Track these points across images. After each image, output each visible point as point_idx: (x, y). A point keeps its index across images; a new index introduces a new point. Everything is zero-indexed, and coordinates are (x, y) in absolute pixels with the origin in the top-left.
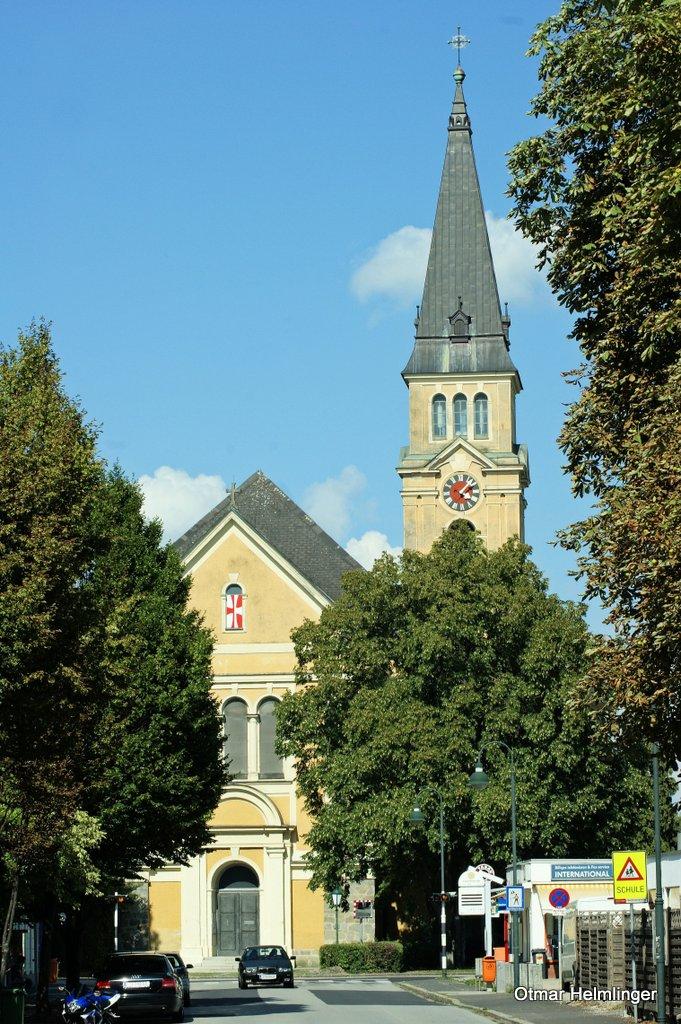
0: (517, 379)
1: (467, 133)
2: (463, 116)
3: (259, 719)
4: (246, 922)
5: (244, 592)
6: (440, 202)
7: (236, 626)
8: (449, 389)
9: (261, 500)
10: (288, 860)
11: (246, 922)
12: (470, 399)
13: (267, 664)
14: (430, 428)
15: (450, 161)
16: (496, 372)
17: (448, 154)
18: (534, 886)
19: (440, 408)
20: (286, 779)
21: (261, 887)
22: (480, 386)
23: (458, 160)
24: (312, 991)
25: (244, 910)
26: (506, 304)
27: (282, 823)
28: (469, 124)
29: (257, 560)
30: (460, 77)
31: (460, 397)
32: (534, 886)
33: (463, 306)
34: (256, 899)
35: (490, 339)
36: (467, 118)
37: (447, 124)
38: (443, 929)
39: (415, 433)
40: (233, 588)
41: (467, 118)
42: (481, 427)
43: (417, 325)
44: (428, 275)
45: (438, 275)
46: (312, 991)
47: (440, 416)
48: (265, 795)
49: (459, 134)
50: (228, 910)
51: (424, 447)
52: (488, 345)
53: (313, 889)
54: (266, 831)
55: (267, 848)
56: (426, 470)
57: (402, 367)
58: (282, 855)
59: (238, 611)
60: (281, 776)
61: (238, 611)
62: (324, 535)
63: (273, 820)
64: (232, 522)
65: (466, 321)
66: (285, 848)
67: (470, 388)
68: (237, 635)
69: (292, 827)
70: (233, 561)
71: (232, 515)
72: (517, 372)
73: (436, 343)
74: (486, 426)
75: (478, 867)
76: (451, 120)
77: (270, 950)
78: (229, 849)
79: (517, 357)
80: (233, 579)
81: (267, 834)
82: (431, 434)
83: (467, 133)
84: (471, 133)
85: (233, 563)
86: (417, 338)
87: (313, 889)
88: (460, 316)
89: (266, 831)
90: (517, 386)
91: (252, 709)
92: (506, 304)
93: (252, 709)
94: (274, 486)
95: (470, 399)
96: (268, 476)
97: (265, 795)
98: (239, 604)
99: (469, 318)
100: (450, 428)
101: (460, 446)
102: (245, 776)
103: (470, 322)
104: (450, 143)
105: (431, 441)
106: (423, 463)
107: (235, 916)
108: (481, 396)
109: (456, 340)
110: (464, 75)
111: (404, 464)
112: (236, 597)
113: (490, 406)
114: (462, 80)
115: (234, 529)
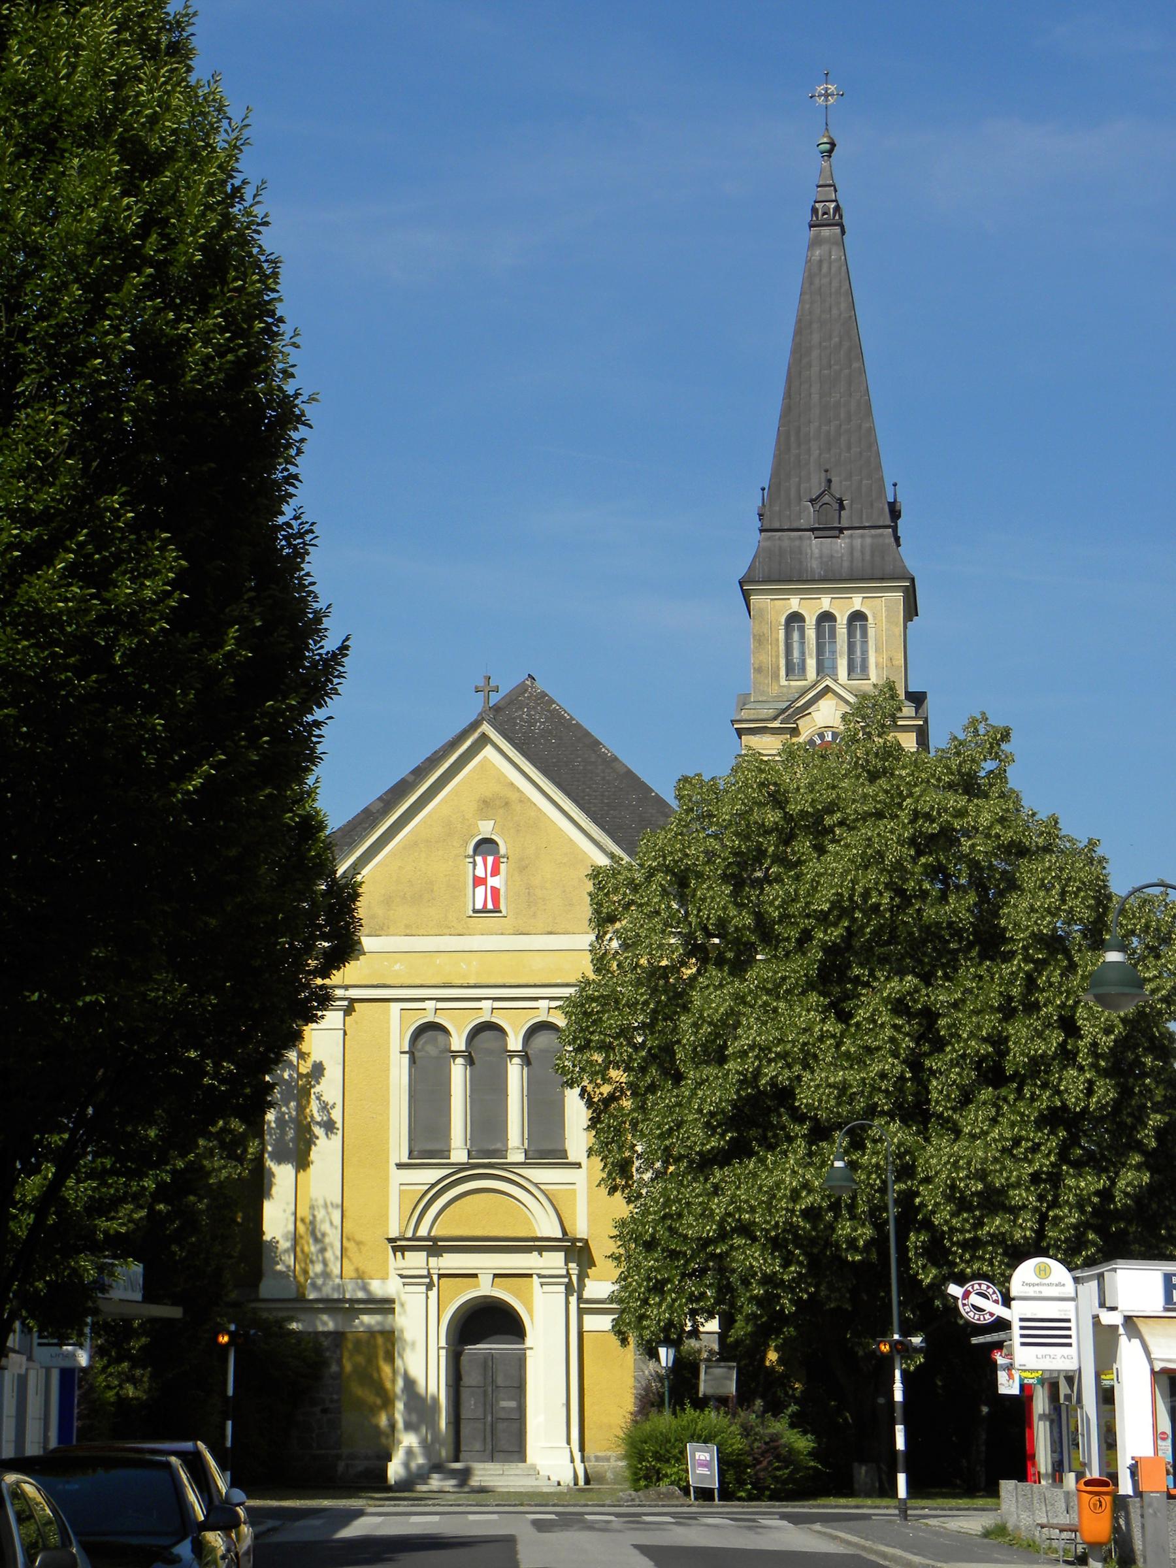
0: (911, 589)
1: (837, 230)
2: (833, 205)
3: (527, 1060)
4: (504, 1404)
5: (502, 851)
6: (798, 332)
7: (490, 906)
8: (811, 607)
9: (531, 723)
10: (573, 1299)
11: (504, 1404)
12: (842, 620)
13: (538, 969)
14: (782, 662)
15: (812, 273)
16: (882, 579)
17: (808, 261)
18: (1128, 1319)
19: (796, 636)
20: (571, 1159)
21: (529, 1341)
22: (857, 602)
23: (825, 269)
24: (636, 1546)
25: (500, 1381)
26: (895, 485)
27: (565, 1232)
28: (841, 217)
29: (524, 800)
30: (828, 147)
31: (826, 618)
32: (1128, 1319)
33: (833, 485)
34: (520, 1362)
35: (873, 532)
36: (837, 209)
37: (807, 216)
38: (898, 1414)
39: (759, 670)
40: (486, 845)
41: (837, 209)
42: (859, 660)
43: (760, 515)
44: (799, 351)
45: (793, 439)
46: (636, 1546)
47: (796, 646)
48: (536, 1185)
49: (826, 232)
50: (474, 1383)
51: (774, 690)
52: (868, 541)
53: (1090, 840)
54: (539, 1245)
55: (539, 1276)
56: (776, 724)
57: (741, 572)
58: (562, 1288)
59: (493, 882)
60: (563, 1154)
61: (493, 882)
62: (630, 774)
63: (549, 1228)
64: (484, 740)
65: (836, 506)
66: (568, 1275)
67: (842, 606)
68: (490, 922)
69: (580, 1240)
70: (485, 802)
71: (486, 728)
72: (913, 580)
73: (790, 538)
74: (865, 661)
75: (968, 1286)
76: (814, 211)
77: (1040, 1372)
78: (475, 1276)
79: (911, 556)
80: (486, 828)
81: (541, 1250)
82: (783, 672)
83: (837, 230)
84: (843, 232)
85: (486, 806)
86: (761, 531)
87: (1090, 840)
88: (826, 498)
89: (539, 1245)
90: (911, 610)
91: (515, 1042)
92: (895, 485)
93: (515, 1042)
94: (552, 702)
95: (842, 620)
96: (541, 686)
97: (536, 1185)
98: (495, 872)
99: (841, 502)
100: (811, 663)
101: (827, 689)
102: (503, 1153)
103: (842, 507)
104: (815, 242)
105: (783, 682)
106: (771, 713)
107: (485, 1392)
108: (857, 617)
109: (818, 533)
110: (833, 145)
111: (744, 714)
112: (490, 859)
113: (871, 632)
114: (831, 151)
115: (488, 751)
